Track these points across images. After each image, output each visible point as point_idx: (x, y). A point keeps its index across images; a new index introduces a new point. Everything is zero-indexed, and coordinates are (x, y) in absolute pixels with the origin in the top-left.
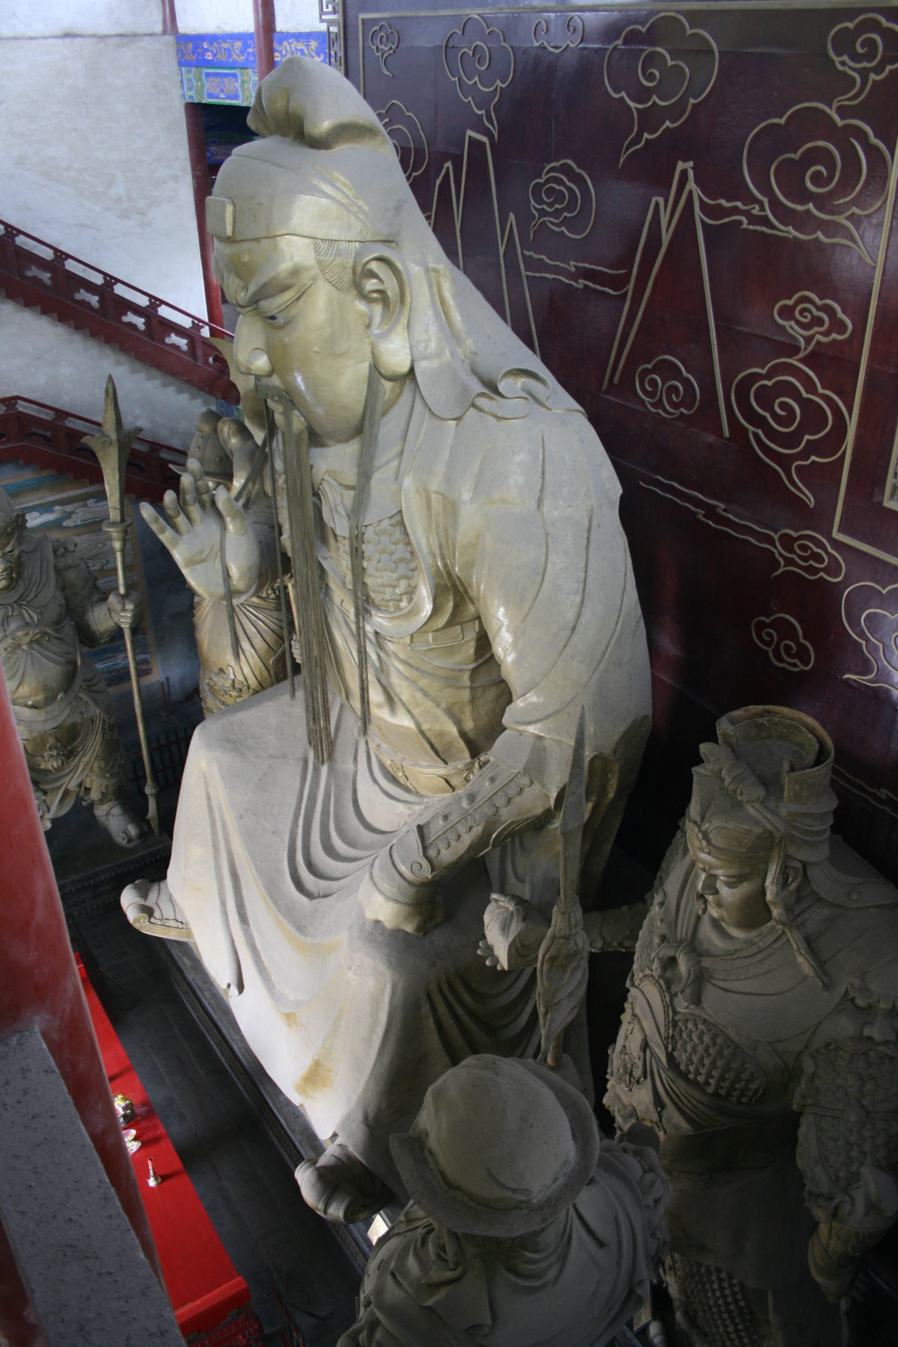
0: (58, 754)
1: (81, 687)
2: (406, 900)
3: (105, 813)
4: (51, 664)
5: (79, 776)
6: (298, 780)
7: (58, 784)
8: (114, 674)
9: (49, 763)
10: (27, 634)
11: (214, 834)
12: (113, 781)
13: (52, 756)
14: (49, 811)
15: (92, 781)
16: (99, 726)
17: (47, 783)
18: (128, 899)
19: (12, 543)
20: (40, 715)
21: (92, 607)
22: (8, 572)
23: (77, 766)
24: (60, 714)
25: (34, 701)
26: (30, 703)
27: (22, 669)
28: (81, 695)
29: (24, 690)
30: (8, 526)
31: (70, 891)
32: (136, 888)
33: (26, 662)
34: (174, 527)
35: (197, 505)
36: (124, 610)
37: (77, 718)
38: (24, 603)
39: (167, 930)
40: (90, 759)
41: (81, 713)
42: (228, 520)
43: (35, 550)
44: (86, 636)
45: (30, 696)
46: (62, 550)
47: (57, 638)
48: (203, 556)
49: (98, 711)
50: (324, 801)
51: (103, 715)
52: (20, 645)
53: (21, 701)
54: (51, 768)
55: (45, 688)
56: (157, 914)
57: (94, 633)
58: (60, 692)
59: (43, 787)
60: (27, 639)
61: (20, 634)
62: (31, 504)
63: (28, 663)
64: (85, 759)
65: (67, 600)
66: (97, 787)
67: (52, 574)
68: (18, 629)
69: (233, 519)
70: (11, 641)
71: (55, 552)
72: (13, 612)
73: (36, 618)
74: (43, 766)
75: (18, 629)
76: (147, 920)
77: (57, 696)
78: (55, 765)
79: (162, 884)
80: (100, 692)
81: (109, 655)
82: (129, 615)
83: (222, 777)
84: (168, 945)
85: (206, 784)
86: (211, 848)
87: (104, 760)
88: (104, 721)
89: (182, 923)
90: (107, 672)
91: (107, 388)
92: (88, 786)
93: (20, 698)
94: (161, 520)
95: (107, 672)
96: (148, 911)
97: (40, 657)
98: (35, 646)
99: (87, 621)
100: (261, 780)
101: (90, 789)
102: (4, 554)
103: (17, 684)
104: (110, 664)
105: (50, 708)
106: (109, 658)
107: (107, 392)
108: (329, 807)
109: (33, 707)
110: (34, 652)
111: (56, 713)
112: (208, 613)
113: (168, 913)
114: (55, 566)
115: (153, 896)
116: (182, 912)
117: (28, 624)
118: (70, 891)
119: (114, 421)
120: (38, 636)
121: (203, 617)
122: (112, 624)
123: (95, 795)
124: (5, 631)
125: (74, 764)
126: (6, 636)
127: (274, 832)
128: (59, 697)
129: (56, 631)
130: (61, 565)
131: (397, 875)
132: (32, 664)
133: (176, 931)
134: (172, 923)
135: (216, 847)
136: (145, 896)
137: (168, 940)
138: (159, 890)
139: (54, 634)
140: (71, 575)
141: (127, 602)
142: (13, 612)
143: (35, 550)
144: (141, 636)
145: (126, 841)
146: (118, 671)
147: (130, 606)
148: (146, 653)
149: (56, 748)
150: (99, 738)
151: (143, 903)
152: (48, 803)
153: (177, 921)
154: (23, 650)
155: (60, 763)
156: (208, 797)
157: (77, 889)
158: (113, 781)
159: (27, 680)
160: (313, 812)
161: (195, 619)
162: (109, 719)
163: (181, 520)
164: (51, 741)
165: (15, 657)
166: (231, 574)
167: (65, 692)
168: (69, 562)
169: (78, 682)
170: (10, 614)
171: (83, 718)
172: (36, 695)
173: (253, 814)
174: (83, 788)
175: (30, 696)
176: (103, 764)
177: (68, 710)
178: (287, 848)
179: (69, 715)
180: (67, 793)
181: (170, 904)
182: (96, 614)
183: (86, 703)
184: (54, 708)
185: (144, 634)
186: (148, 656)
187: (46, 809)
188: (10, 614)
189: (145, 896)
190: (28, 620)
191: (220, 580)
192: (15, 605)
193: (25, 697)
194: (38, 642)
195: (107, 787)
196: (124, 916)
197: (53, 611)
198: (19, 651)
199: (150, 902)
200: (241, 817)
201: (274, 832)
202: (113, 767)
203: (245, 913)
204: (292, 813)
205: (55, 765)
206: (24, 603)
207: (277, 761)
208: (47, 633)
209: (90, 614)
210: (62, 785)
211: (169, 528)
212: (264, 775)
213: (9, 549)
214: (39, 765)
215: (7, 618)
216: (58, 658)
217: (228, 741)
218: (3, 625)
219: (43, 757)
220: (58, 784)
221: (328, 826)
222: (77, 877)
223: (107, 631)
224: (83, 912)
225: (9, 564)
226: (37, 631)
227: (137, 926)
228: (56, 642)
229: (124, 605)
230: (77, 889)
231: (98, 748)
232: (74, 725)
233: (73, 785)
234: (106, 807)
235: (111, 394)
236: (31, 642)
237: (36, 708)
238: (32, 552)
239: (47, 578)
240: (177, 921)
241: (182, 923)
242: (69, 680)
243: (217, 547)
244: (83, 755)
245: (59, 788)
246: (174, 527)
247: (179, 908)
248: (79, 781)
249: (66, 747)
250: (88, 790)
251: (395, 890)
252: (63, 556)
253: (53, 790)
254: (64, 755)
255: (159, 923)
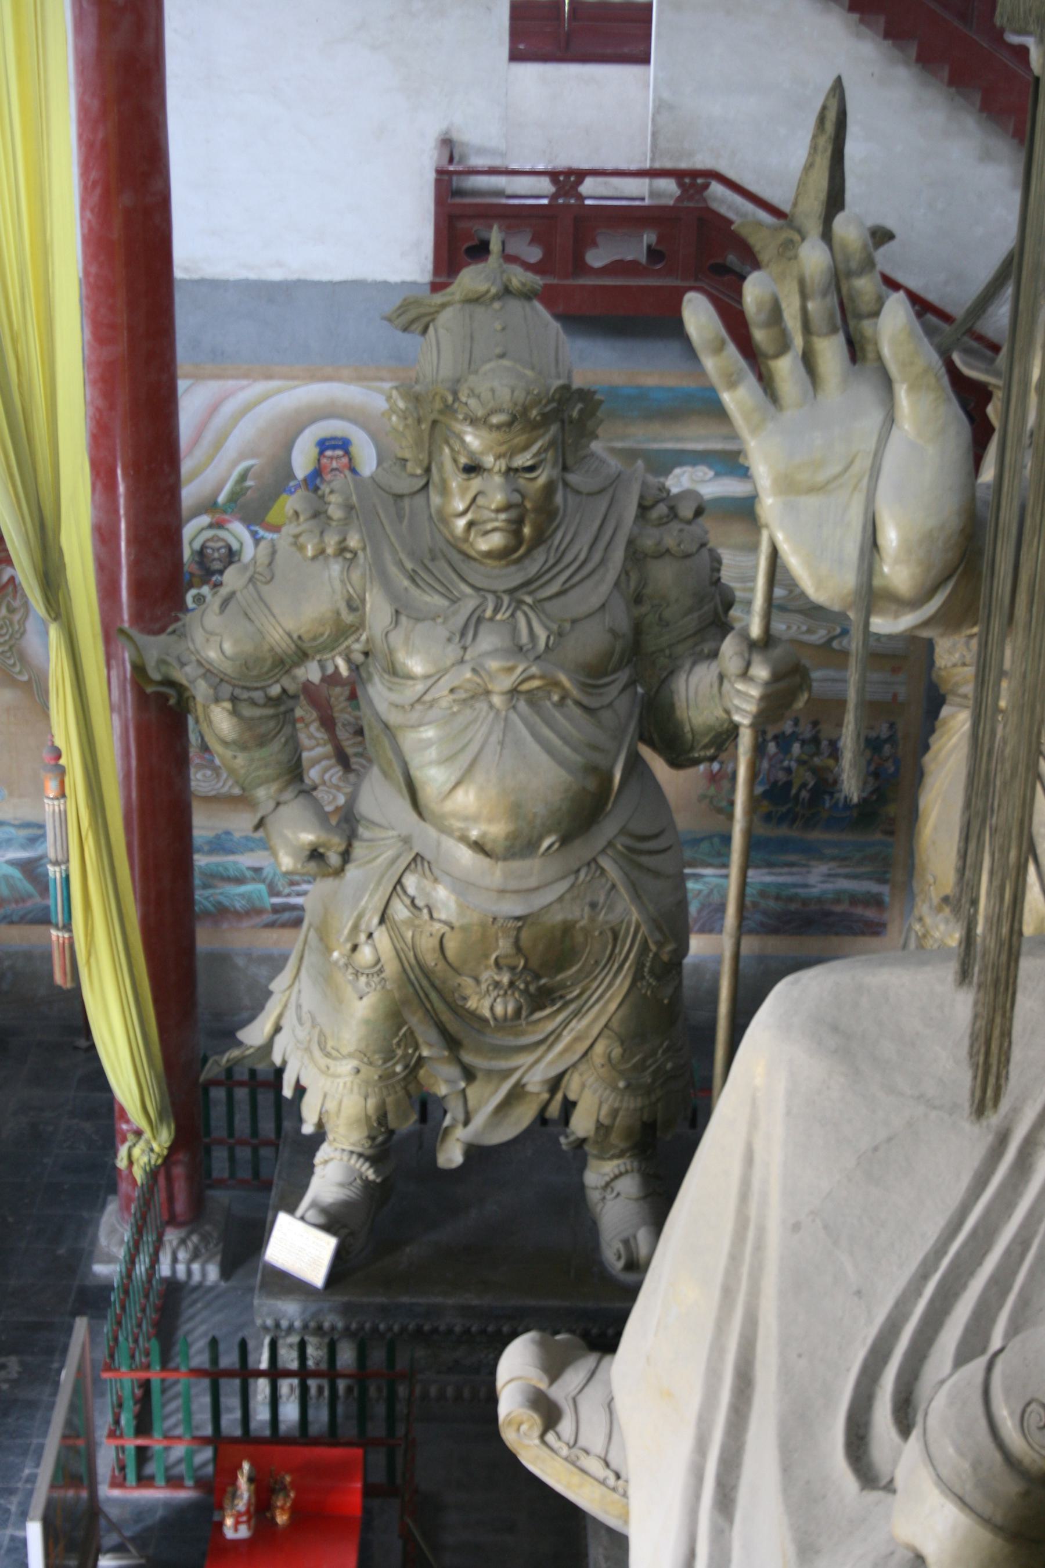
0: (512, 984)
1: (610, 844)
2: (998, 1519)
3: (602, 1183)
4: (544, 758)
5: (551, 1063)
6: (966, 1180)
7: (503, 1064)
8: (793, 907)
9: (487, 1002)
10: (511, 670)
11: (735, 1257)
12: (631, 1103)
13: (497, 984)
14: (466, 1123)
15: (583, 1086)
16: (628, 952)
17: (479, 1050)
18: (517, 1365)
19: (535, 448)
20: (494, 873)
21: (694, 664)
22: (513, 514)
23: (555, 1036)
24: (538, 888)
25: (484, 835)
26: (474, 834)
27: (474, 748)
28: (606, 863)
29: (466, 799)
30: (536, 402)
31: (450, 1331)
32: (543, 1345)
33: (490, 733)
34: (766, 381)
35: (839, 339)
36: (745, 675)
37: (577, 913)
38: (529, 600)
39: (577, 1478)
40: (589, 1026)
41: (593, 905)
42: (902, 394)
43: (601, 491)
44: (660, 728)
45: (475, 819)
46: (662, 509)
47: (578, 703)
48: (821, 477)
49: (635, 916)
50: (1008, 1252)
51: (643, 929)
52: (488, 693)
53: (458, 824)
54: (487, 1013)
55: (515, 810)
56: (566, 1426)
57: (678, 725)
58: (549, 832)
59: (468, 1058)
60: (507, 682)
61: (494, 665)
62: (700, 446)
63: (494, 739)
64: (578, 1026)
65: (638, 629)
66: (591, 1107)
67: (618, 555)
68: (493, 653)
69: (912, 389)
70: (469, 675)
71: (644, 509)
72: (496, 610)
73: (542, 635)
74: (472, 1004)
75: (493, 653)
76: (536, 1432)
77: (541, 839)
78: (499, 1010)
79: (607, 1359)
80: (656, 874)
81: (792, 858)
82: (755, 692)
83: (788, 1113)
84: (590, 1532)
85: (753, 1124)
86: (716, 1294)
87: (622, 1043)
88: (645, 948)
89: (618, 1476)
90: (778, 898)
91: (824, 108)
92: (572, 1097)
93: (455, 815)
94: (732, 349)
95: (778, 898)
96: (548, 1413)
97: (525, 733)
98: (522, 705)
99: (672, 692)
100: (875, 1149)
101: (574, 1104)
102: (509, 469)
103: (453, 780)
104: (789, 879)
105: (516, 865)
106: (792, 865)
107: (821, 119)
108: (1014, 1273)
109: (478, 847)
110: (514, 716)
111: (533, 882)
112: (955, 746)
113: (593, 1437)
114: (630, 542)
115: (573, 1378)
116: (623, 1448)
117: (521, 648)
118: (450, 1331)
119: (823, 196)
120: (536, 683)
121: (944, 753)
122: (720, 713)
123: (582, 1124)
124: (465, 649)
125: (550, 1026)
126: (462, 661)
127: (859, 1293)
128: (546, 844)
129: (584, 687)
130: (648, 543)
131: (983, 1423)
132: (502, 743)
133: (599, 1491)
134: (594, 1466)
135: (728, 1293)
136: (554, 1369)
137: (594, 1520)
138: (593, 1374)
139: (575, 692)
140: (664, 575)
141: (757, 658)
142: (496, 610)
143: (601, 491)
144: (878, 836)
145: (620, 1265)
146: (805, 902)
147: (761, 672)
148: (882, 880)
149: (512, 969)
150: (622, 984)
151: (543, 1386)
152: (472, 1103)
153: (607, 1465)
154: (491, 706)
155: (510, 1009)
156: (749, 1159)
157: (467, 1331)
158: (631, 1103)
159: (479, 776)
160: (972, 1273)
161: (928, 758)
162: (660, 945)
163: (785, 368)
164: (504, 946)
165: (468, 714)
166: (881, 541)
167: (565, 840)
168: (670, 542)
169: (609, 828)
170: (488, 613)
171: (592, 919)
172: (490, 821)
173: (826, 1227)
174: (559, 1097)
175: (475, 819)
176: (617, 1052)
177: (562, 887)
178: (869, 1342)
179: (561, 899)
180: (517, 1094)
181: (604, 1417)
182: (694, 679)
183: (614, 886)
184: (531, 869)
185: (891, 833)
186: (885, 889)
187: (461, 1117)
188: (488, 613)
189: (554, 1369)
190: (524, 638)
191: (852, 549)
192: (506, 599)
193: (466, 819)
194: (532, 699)
195: (614, 1113)
196: (493, 1399)
197: (591, 641)
198: (482, 706)
199: (560, 1392)
200: (796, 1227)
201: (859, 1293)
202: (640, 1067)
203: (734, 1488)
204: (920, 1256)
205: (499, 1010)
206: (529, 600)
207: (933, 1114)
208: (557, 684)
209: (683, 677)
210: (510, 1072)
211: (751, 379)
212: (889, 1140)
213: (523, 460)
214: (465, 999)
215: (479, 620)
216: (567, 751)
217: (835, 1029)
218: (463, 634)
219: (477, 981)
220: (503, 1064)
221: (992, 1320)
222: (475, 1302)
223: (711, 728)
224: (466, 1393)
225: (516, 498)
226: (534, 670)
227: (509, 1436)
228: (577, 711)
229: (748, 665)
230: (467, 1331)
231: (613, 1006)
232: (567, 928)
233: (536, 1080)
234: (610, 1167)
235: (830, 126)
236: (513, 692)
237: (487, 854)
238: (590, 494)
239: (603, 562)
240: (607, 1465)
241: (618, 1476)
242: (583, 813)
243: (863, 464)
244: (576, 1014)
245: (507, 1074)
246: (766, 381)
247: (620, 1428)
248: (553, 1072)
249: (537, 977)
250: (569, 1106)
251: (966, 1465)
252: (661, 523)
253: (490, 1073)
254: (526, 992)
255: (565, 1451)
